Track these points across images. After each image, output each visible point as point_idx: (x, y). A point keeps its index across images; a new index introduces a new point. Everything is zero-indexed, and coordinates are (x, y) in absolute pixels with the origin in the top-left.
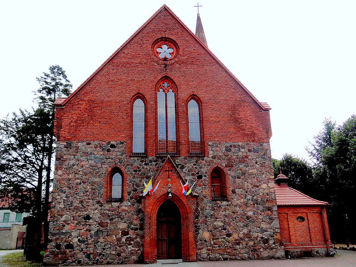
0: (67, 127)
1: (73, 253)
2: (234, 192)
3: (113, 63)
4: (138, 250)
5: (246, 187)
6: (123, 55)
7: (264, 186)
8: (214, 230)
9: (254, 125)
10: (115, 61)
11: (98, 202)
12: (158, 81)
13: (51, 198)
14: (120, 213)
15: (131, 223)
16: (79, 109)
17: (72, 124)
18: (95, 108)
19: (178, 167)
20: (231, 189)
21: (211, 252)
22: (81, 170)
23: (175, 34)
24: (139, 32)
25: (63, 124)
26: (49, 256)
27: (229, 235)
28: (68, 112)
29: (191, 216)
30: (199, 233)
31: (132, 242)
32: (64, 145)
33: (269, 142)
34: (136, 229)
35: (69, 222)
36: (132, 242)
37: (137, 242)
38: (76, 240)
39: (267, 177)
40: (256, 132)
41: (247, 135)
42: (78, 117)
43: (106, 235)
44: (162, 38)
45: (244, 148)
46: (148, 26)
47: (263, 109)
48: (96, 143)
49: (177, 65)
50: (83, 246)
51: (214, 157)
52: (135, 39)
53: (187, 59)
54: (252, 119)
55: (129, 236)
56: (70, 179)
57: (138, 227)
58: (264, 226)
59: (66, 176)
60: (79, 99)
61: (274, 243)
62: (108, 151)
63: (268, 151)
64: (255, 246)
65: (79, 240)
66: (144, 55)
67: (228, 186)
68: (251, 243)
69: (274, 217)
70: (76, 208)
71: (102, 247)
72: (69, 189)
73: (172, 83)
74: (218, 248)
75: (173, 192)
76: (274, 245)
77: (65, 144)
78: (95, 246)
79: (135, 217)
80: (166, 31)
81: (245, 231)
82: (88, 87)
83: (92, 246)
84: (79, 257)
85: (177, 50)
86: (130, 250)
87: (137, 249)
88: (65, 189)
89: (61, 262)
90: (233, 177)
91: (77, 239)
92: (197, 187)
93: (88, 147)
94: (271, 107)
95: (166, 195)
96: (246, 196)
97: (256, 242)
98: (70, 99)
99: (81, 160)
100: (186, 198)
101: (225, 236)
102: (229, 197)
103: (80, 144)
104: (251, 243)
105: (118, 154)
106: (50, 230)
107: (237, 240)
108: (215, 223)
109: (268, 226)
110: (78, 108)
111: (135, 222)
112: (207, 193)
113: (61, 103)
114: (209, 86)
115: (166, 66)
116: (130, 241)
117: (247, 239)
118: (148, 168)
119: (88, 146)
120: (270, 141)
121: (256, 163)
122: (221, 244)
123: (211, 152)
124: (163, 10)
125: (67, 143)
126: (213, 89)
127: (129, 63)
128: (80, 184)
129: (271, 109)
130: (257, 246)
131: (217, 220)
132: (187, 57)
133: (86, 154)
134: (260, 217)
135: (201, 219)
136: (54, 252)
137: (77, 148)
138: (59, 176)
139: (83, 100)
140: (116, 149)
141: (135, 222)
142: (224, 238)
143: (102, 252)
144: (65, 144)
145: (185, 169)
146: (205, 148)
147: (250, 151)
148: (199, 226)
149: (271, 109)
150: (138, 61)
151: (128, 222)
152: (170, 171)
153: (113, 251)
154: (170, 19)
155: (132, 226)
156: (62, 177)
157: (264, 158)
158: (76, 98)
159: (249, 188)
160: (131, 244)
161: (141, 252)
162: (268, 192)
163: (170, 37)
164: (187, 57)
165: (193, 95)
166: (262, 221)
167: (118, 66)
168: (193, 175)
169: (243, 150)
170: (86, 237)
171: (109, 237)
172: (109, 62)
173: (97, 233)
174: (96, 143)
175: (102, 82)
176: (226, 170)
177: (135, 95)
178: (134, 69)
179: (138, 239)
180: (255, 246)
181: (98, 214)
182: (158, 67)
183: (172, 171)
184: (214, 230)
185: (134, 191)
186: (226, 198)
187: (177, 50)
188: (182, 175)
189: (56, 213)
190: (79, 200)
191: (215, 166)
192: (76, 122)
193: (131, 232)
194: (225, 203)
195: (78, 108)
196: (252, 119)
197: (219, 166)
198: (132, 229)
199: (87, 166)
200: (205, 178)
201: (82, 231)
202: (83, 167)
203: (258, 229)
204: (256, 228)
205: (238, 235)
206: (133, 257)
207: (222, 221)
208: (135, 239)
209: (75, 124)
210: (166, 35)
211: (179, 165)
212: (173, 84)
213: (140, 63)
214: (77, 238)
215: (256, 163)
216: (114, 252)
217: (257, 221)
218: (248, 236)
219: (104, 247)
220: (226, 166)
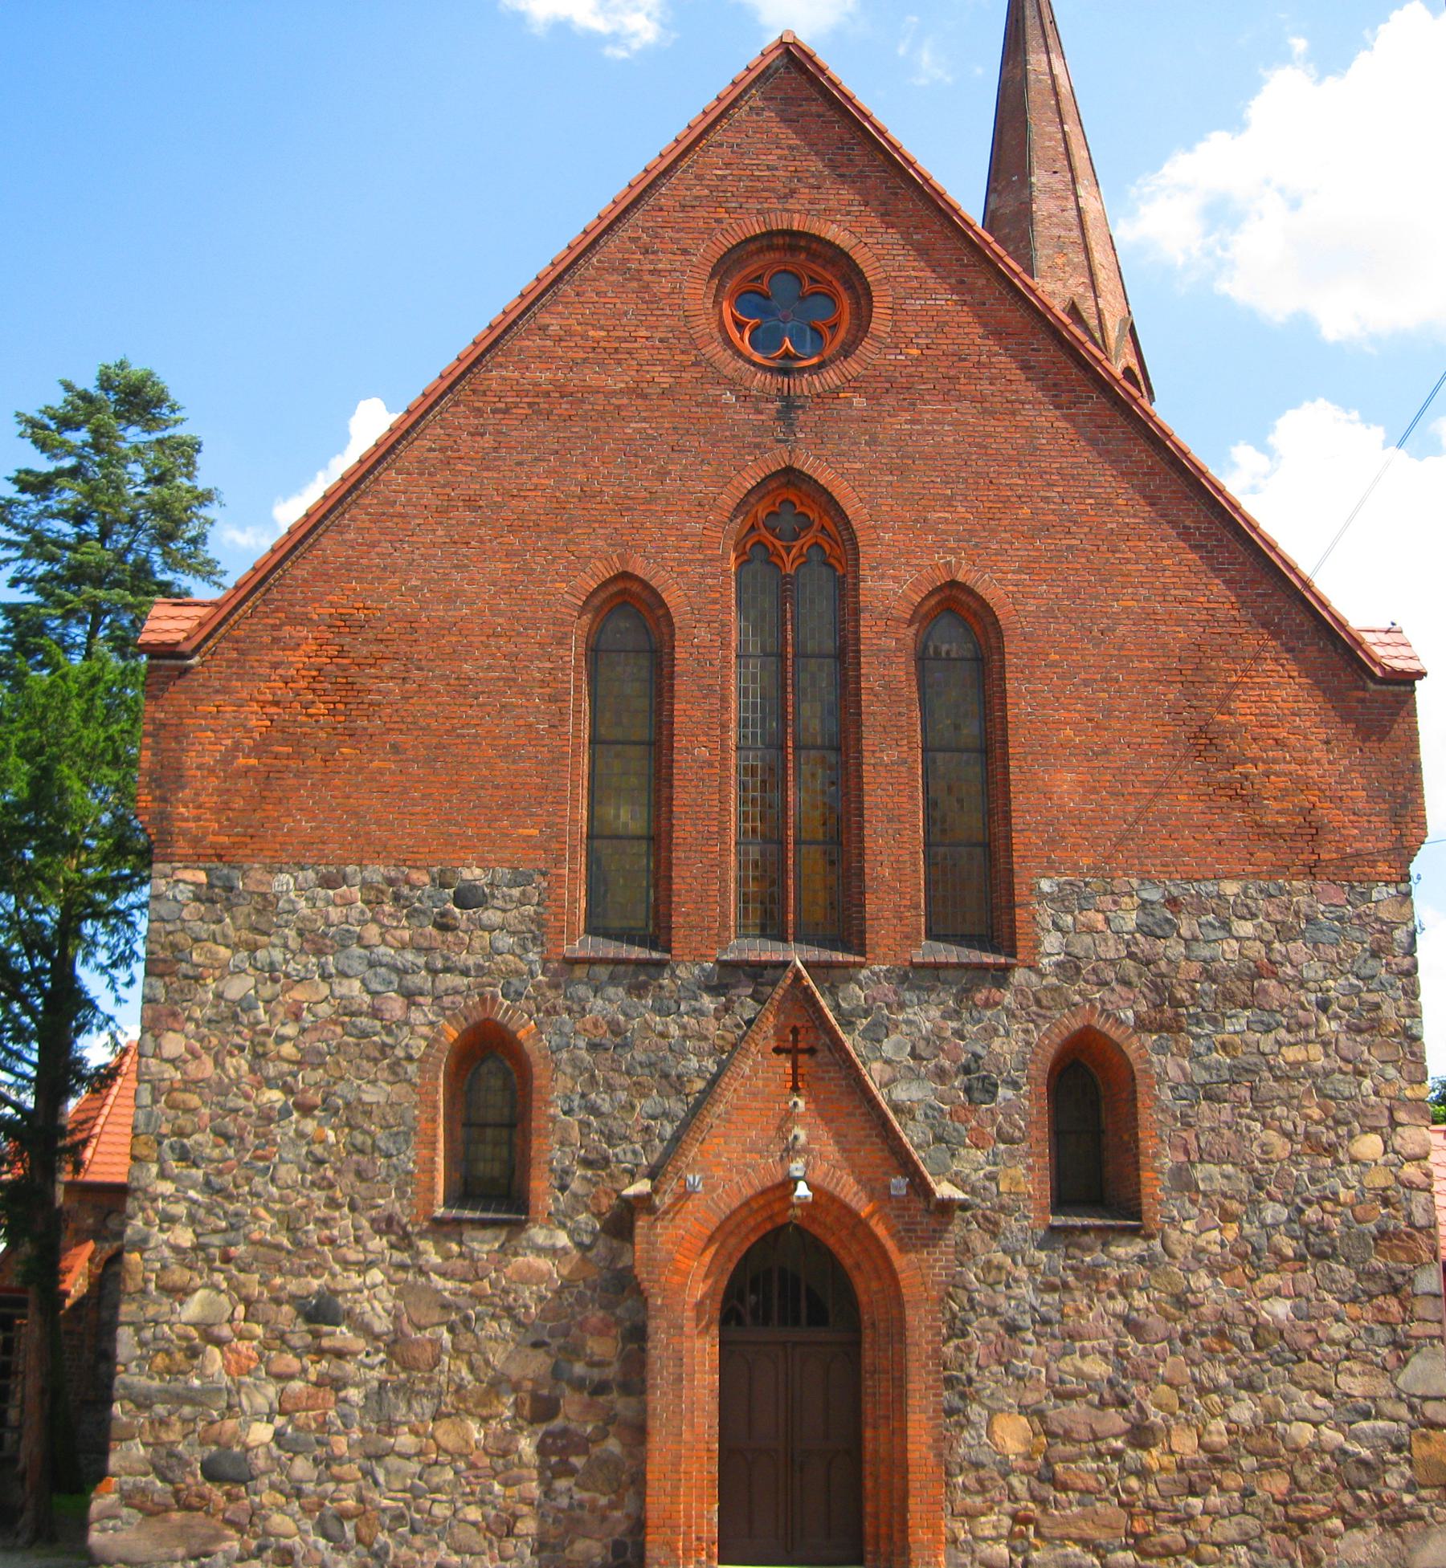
0: (213, 782)
1: (247, 1502)
2: (1183, 1181)
3: (474, 391)
4: (612, 1506)
5: (1257, 1150)
6: (535, 342)
7: (1369, 1146)
8: (1056, 1407)
9: (1314, 772)
10: (494, 377)
11: (387, 1225)
12: (743, 502)
13: (122, 1120)
14: (506, 1292)
15: (574, 1351)
16: (280, 671)
17: (241, 761)
18: (371, 666)
19: (848, 1025)
20: (1168, 1160)
21: (1037, 1533)
22: (290, 1030)
23: (848, 213)
24: (634, 204)
25: (190, 760)
26: (116, 1517)
27: (1141, 1435)
28: (217, 691)
29: (920, 1323)
30: (968, 1420)
31: (578, 1461)
32: (191, 888)
33: (1406, 878)
34: (601, 1388)
35: (225, 1331)
36: (578, 1461)
37: (605, 1462)
38: (261, 1433)
39: (1388, 1090)
40: (1327, 813)
41: (1264, 833)
42: (272, 721)
43: (428, 1412)
44: (770, 234)
45: (1254, 916)
46: (684, 164)
47: (1372, 675)
48: (376, 872)
49: (859, 402)
50: (302, 1467)
51: (1070, 967)
52: (612, 244)
53: (917, 362)
54: (1306, 738)
55: (558, 1423)
56: (229, 1087)
57: (612, 1372)
58: (1355, 1384)
59: (206, 1069)
60: (277, 610)
61: (1411, 1486)
62: (444, 925)
63: (1400, 934)
64: (1296, 1502)
65: (278, 1435)
66: (661, 340)
67: (1148, 1144)
68: (1279, 1484)
69: (1416, 1328)
70: (268, 1256)
71: (409, 1481)
72: (222, 1141)
73: (827, 513)
74: (1076, 1509)
75: (817, 1178)
76: (1407, 1499)
77: (202, 877)
78: (367, 1473)
79: (596, 1315)
80: (793, 192)
81: (1244, 1411)
82: (328, 544)
83: (352, 1470)
84: (281, 1530)
85: (858, 303)
86: (564, 1502)
87: (603, 1501)
88: (202, 1140)
89: (180, 1552)
90: (1181, 1091)
91: (271, 1428)
92: (963, 1151)
93: (329, 902)
94: (1424, 664)
95: (778, 1193)
96: (1255, 1203)
97: (1304, 1478)
98: (231, 614)
99: (287, 975)
100: (898, 1216)
101: (1118, 1444)
102: (1154, 1216)
103: (284, 881)
104: (1279, 1484)
105: (499, 944)
106: (120, 1368)
107: (1194, 1465)
108: (1066, 1364)
109: (1382, 1387)
110: (275, 666)
111: (597, 1347)
112: (1022, 1188)
113: (181, 636)
114: (1047, 528)
115: (789, 406)
116: (564, 1452)
117: (1249, 1462)
118: (674, 1031)
119: (331, 893)
120: (1413, 869)
121: (1323, 1005)
122: (1095, 1484)
123: (1052, 942)
124: (774, 66)
125: (208, 872)
126: (1070, 547)
127: (571, 394)
128: (285, 1113)
129: (1421, 675)
130: (1307, 1502)
131: (1078, 1344)
132: (915, 352)
133: (314, 942)
134: (1338, 1331)
135: (982, 1333)
136: (143, 1491)
137: (267, 903)
138: (168, 1066)
139: (304, 620)
140: (491, 916)
141: (597, 1347)
142: (1117, 1455)
143: (409, 1508)
144: (202, 877)
145: (894, 1037)
146: (1020, 914)
147: (1284, 932)
148: (970, 1380)
149: (1421, 675)
150: (617, 380)
151: (556, 1343)
152: (803, 1051)
153: (468, 1504)
154: (819, 116)
155: (579, 1368)
156: (184, 1073)
157: (1373, 977)
158: (262, 608)
159: (1273, 1156)
160: (570, 1471)
161: (628, 1516)
162: (1391, 1181)
163: (816, 227)
164: (915, 352)
165: (953, 584)
166: (1347, 1358)
167: (506, 411)
168: (941, 1074)
169: (1245, 928)
170: (320, 1419)
171: (445, 1424)
172: (451, 388)
173: (380, 1403)
174: (376, 872)
175: (410, 510)
176: (1140, 1048)
177: (604, 585)
178: (596, 431)
179: (613, 1445)
180: (1296, 1502)
181: (383, 1293)
182: (743, 414)
183: (812, 1051)
184: (1056, 1407)
185: (587, 1163)
186: (1137, 1215)
187: (858, 303)
188: (874, 1074)
189: (154, 1276)
190: (277, 1206)
191: (1077, 1024)
192: (258, 750)
193: (572, 1405)
194: (1124, 1250)
195: (275, 666)
196: (1306, 738)
197: (1099, 1023)
198: (578, 1385)
199: (324, 1009)
200: (1010, 1094)
201: (297, 1385)
202: (297, 1017)
203: (1320, 1401)
204: (1310, 1400)
205: (1199, 1437)
206: (581, 1545)
207: (1104, 1354)
208: (594, 1442)
209: (253, 762)
210: (796, 216)
211: (852, 1013)
212: (831, 518)
213: (637, 392)
214: (270, 1421)
215: (1325, 1011)
216: (473, 1513)
217: (1316, 1353)
218: (1255, 1442)
219: (420, 1478)
220: (1142, 1025)
